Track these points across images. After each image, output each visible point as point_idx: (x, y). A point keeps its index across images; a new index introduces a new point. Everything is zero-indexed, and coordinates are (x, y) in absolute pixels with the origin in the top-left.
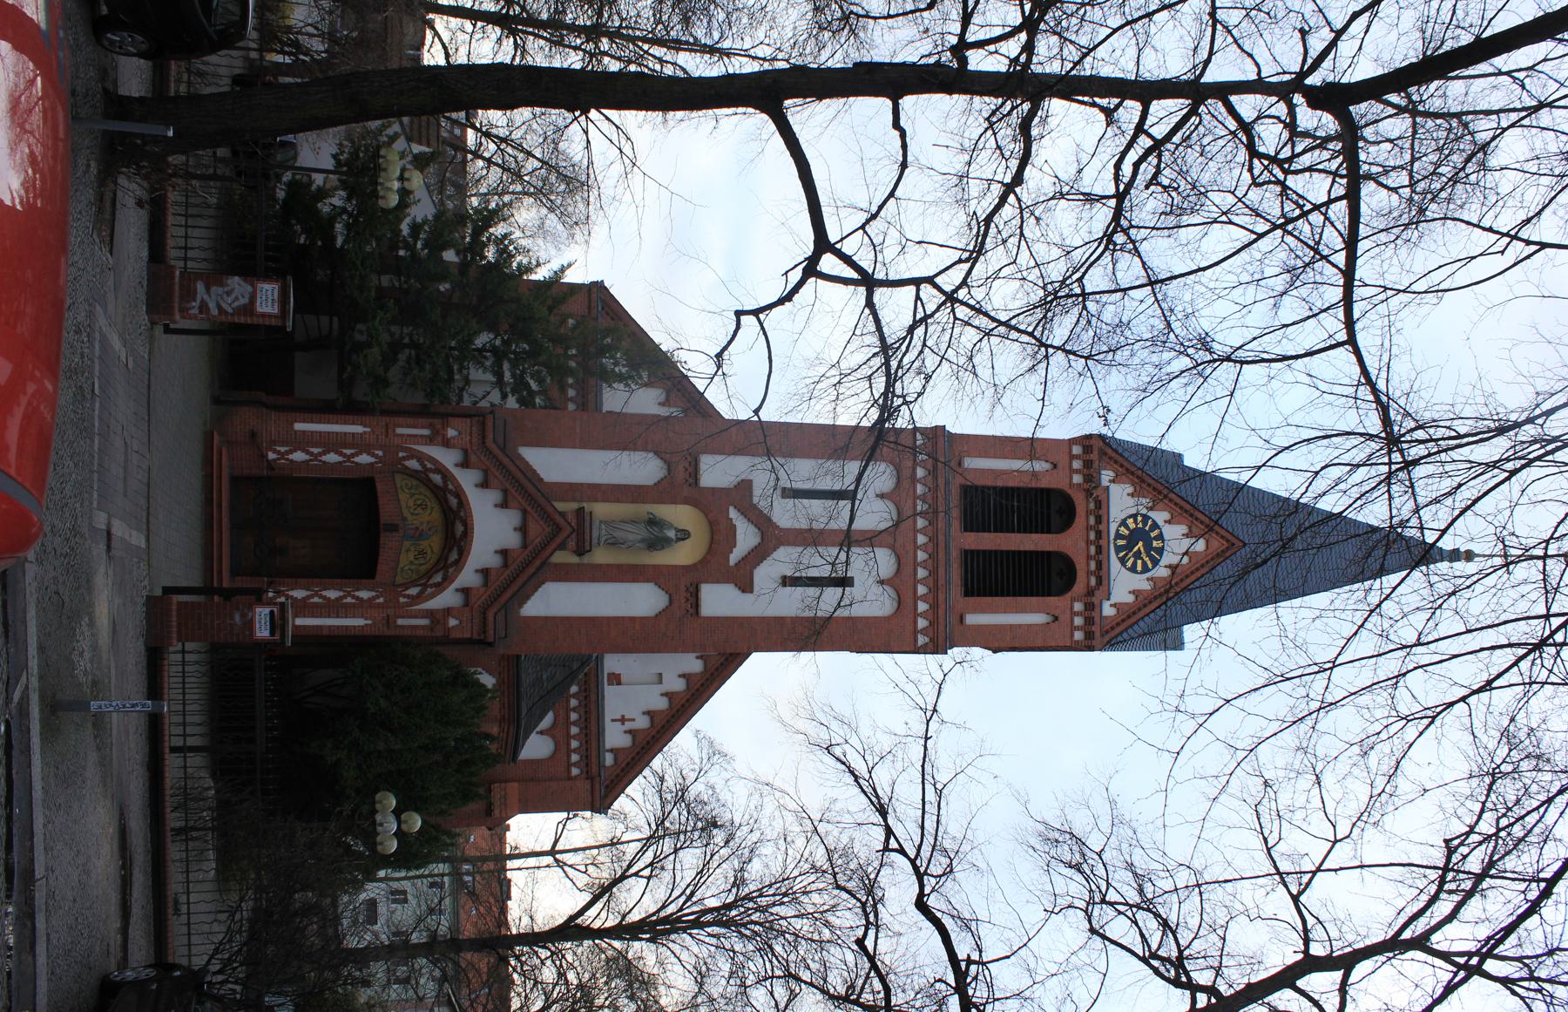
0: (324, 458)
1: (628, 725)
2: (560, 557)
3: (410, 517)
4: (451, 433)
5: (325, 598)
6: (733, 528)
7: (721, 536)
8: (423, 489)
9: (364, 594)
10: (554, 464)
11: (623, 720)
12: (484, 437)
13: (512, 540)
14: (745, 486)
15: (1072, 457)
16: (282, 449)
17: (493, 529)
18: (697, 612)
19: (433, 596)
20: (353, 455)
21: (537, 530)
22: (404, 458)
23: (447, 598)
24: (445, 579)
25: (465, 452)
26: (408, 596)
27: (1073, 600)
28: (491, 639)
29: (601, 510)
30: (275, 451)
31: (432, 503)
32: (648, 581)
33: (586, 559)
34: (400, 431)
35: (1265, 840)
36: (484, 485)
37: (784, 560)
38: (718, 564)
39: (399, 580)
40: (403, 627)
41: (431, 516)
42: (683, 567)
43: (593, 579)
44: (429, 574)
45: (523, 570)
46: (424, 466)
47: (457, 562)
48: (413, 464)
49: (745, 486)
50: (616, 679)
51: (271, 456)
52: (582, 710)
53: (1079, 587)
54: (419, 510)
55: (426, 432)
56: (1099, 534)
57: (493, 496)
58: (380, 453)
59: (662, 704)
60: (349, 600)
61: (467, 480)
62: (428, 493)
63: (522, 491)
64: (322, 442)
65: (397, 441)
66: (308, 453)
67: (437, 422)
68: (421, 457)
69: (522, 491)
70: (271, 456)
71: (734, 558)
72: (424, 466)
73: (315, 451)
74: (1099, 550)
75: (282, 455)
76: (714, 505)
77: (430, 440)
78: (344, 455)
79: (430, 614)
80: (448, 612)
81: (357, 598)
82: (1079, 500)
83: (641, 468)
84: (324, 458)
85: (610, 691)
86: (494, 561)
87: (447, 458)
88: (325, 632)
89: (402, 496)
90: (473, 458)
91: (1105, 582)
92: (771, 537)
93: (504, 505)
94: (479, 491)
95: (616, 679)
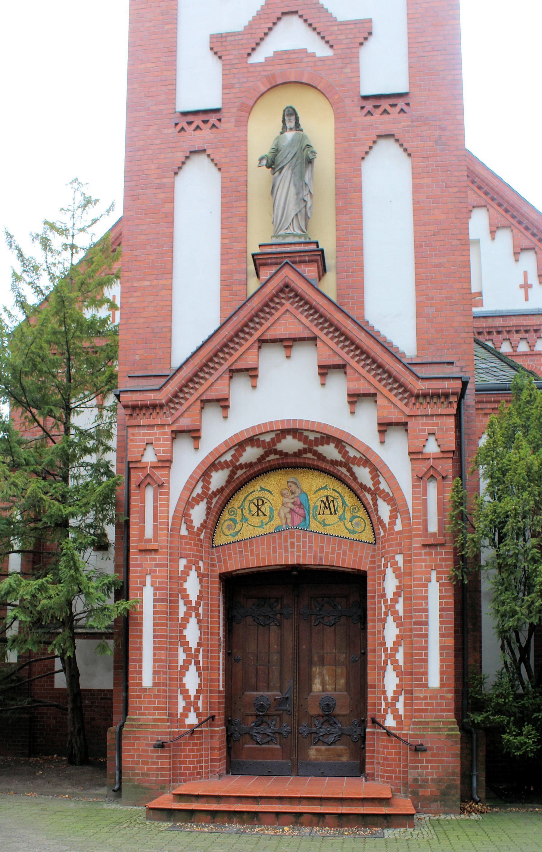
0: (193, 645)
1: (533, 279)
3: (276, 522)
4: (150, 457)
5: (397, 644)
6: (279, 55)
7: (289, 77)
8: (235, 503)
9: (391, 584)
10: (195, 315)
11: (526, 286)
12: (154, 406)
13: (305, 361)
14: (219, 45)
16: (182, 704)
17: (289, 392)
19: (391, 479)
20: (187, 602)
21: (288, 322)
22: (190, 527)
23: (395, 456)
24: (366, 462)
25: (176, 434)
26: (393, 517)
28: (458, 385)
29: (258, 235)
30: (185, 715)
31: (255, 489)
32: (359, 174)
34: (149, 533)
36: (223, 404)
39: (367, 536)
40: (441, 523)
41: (272, 488)
42: (337, 119)
43: (359, 250)
44: (356, 490)
45: (351, 350)
46: (200, 498)
48: (198, 514)
49: (219, 45)
51: (192, 719)
52: (516, 337)
54: (265, 509)
55: (149, 493)
57: (239, 391)
58: (183, 562)
59: (505, 238)
60: (400, 607)
61: (218, 431)
62: (241, 496)
63: (230, 353)
64: (174, 660)
65: (163, 537)
66: (185, 668)
67: (137, 476)
68: (189, 503)
69: (230, 353)
70: (192, 719)
71: (321, 50)
72: (200, 498)
73: (182, 656)
75: (190, 704)
76: (243, 98)
77: (161, 487)
78: (187, 615)
79: (420, 480)
80: (415, 454)
81: (397, 594)
83: (197, 193)
84: (193, 645)
86: (339, 387)
87: (187, 461)
88: (450, 641)
89: (247, 532)
90: (185, 423)
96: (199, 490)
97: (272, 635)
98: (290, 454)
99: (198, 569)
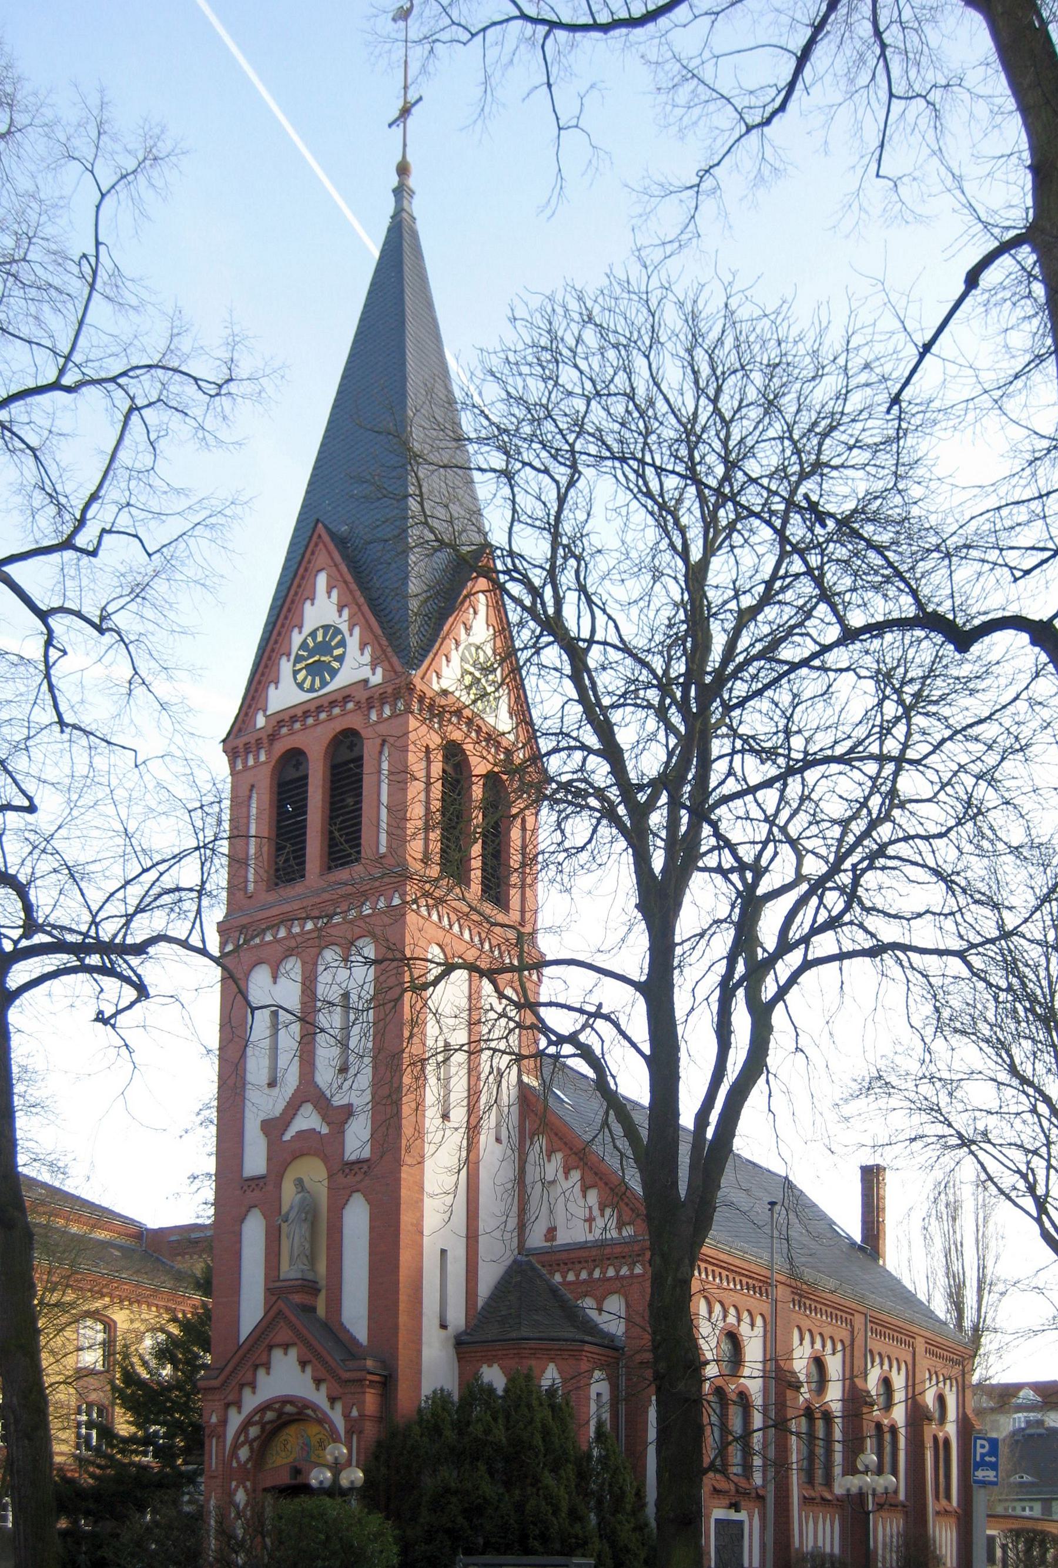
1: (596, 1212)
2: (321, 1311)
4: (214, 1419)
15: (246, 768)
17: (285, 1378)
18: (367, 1161)
22: (238, 1462)
27: (368, 724)
29: (288, 1270)
33: (323, 1283)
35: (124, 374)
36: (253, 1385)
37: (325, 1076)
38: (324, 1147)
46: (243, 1444)
47: (314, 1411)
48: (244, 1453)
50: (551, 1233)
52: (578, 1266)
53: (354, 721)
54: (289, 1447)
56: (319, 709)
58: (234, 1484)
61: (251, 1401)
68: (236, 1447)
74: (333, 704)
80: (346, 1416)
82: (280, 747)
85: (563, 1238)
87: (235, 1420)
90: (231, 1398)
91: (347, 692)
92: (306, 1093)
93: (267, 1366)
94: (258, 1390)
95: (551, 1233)
96: (242, 1438)
97: (811, 1544)
98: (286, 1416)
99: (245, 1487)
